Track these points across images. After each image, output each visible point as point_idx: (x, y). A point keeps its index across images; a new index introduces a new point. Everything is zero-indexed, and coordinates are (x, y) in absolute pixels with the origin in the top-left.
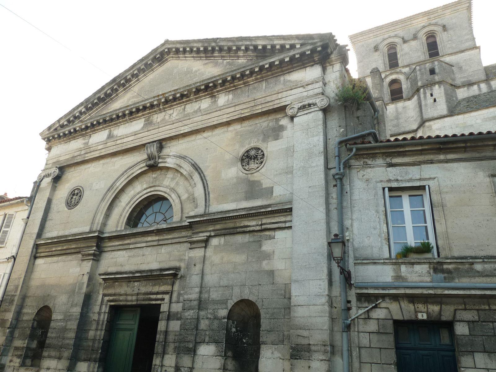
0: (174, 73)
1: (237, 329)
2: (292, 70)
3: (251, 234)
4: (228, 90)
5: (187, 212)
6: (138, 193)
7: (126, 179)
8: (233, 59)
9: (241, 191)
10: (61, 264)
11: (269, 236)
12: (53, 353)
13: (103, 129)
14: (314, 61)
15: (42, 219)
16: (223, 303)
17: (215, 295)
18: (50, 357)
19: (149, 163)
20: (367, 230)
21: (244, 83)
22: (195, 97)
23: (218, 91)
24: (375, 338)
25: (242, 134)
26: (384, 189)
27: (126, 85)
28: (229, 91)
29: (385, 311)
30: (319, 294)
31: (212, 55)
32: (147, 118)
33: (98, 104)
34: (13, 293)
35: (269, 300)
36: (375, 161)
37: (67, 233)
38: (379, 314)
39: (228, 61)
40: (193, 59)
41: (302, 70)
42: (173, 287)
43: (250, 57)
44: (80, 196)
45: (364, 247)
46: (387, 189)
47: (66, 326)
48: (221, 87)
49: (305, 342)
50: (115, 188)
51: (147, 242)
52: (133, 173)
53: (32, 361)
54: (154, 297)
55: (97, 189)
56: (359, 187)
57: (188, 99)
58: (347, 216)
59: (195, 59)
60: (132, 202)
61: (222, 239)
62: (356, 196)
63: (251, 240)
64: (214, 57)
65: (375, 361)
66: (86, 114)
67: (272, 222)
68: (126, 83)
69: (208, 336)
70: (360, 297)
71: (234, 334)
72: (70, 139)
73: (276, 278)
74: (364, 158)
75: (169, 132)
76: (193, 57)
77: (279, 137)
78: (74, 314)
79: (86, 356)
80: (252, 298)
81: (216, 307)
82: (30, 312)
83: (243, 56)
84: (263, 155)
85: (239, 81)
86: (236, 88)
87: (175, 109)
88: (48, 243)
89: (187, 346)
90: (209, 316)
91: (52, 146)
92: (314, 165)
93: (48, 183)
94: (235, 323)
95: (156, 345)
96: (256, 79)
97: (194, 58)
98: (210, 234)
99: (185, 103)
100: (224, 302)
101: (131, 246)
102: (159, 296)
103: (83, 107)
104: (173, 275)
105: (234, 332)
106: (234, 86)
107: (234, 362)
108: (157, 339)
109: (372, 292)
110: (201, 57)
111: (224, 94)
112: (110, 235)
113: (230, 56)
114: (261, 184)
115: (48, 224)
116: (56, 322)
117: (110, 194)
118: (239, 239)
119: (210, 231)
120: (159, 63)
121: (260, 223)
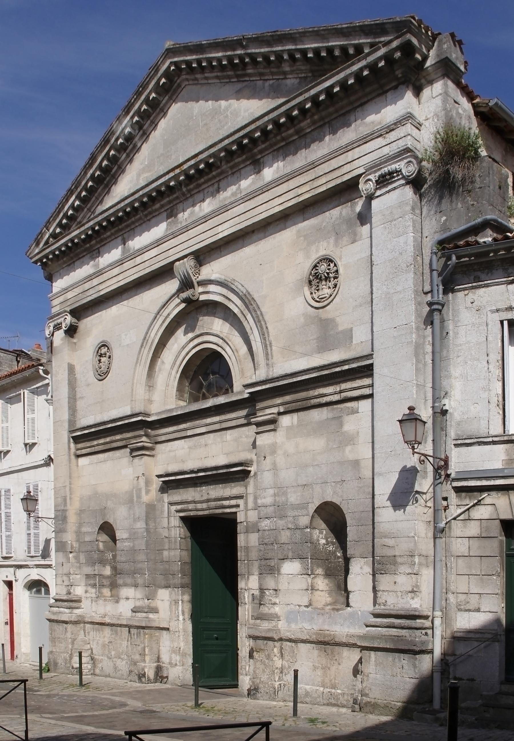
0: (195, 114)
1: (327, 541)
2: (366, 99)
3: (330, 408)
4: (275, 148)
5: (249, 374)
6: (184, 348)
7: (161, 325)
8: (278, 79)
9: (311, 338)
10: (109, 464)
11: (351, 409)
12: (129, 580)
13: (113, 237)
14: (397, 78)
15: (69, 398)
16: (303, 508)
17: (293, 498)
18: (126, 585)
19: (184, 295)
20: (474, 393)
21: (297, 132)
22: (229, 165)
23: (261, 152)
24: (475, 543)
25: (305, 233)
26: (502, 322)
27: (128, 147)
28: (278, 150)
29: (490, 508)
30: (406, 491)
31: (243, 72)
32: (169, 210)
33: (97, 189)
34: (62, 508)
35: (354, 501)
36: (492, 274)
37: (106, 418)
38: (482, 512)
39: (271, 82)
40: (218, 81)
41: (380, 98)
42: (246, 489)
43: (302, 73)
44: (110, 357)
45: (469, 419)
46: (506, 323)
47: (134, 546)
48: (263, 142)
49: (389, 552)
50: (150, 341)
51: (207, 425)
52: (169, 315)
53: (111, 591)
54: (226, 503)
55: (128, 345)
56: (466, 323)
57: (219, 170)
58: (447, 373)
59: (222, 81)
60: (178, 363)
61: (295, 416)
62: (462, 339)
63: (330, 415)
64: (249, 75)
65: (474, 572)
66: (83, 210)
67: (353, 387)
68: (128, 143)
69: (291, 551)
70: (458, 490)
71: (323, 546)
72: (72, 258)
73: (362, 470)
74: (475, 270)
75: (209, 234)
76: (217, 77)
77: (357, 238)
78: (140, 530)
79: (166, 582)
80: (336, 500)
81: (297, 514)
82: (90, 531)
83: (292, 72)
84: (337, 271)
85: (288, 129)
86: (287, 141)
87: (206, 191)
88: (327, 369)
89: (268, 564)
90: (290, 526)
91: (52, 273)
92: (399, 288)
93: (62, 339)
94: (324, 532)
95: (239, 565)
96: (314, 123)
97: (219, 79)
98: (279, 410)
99: (218, 179)
100: (303, 506)
101: (189, 433)
102: (233, 502)
103: (74, 197)
104: (236, 474)
105: (324, 544)
106: (283, 139)
107: (326, 581)
108: (239, 558)
109: (473, 485)
110: (229, 77)
111: (270, 156)
112: (159, 418)
113: (273, 74)
114: (337, 325)
115: (80, 404)
116: (122, 542)
117: (146, 351)
118: (316, 415)
119: (278, 405)
120: (169, 95)
121: (338, 390)
